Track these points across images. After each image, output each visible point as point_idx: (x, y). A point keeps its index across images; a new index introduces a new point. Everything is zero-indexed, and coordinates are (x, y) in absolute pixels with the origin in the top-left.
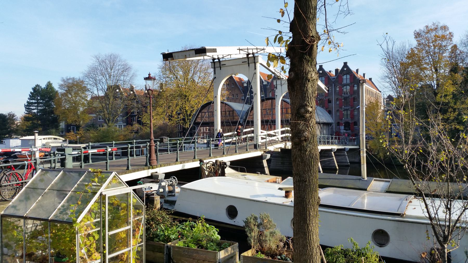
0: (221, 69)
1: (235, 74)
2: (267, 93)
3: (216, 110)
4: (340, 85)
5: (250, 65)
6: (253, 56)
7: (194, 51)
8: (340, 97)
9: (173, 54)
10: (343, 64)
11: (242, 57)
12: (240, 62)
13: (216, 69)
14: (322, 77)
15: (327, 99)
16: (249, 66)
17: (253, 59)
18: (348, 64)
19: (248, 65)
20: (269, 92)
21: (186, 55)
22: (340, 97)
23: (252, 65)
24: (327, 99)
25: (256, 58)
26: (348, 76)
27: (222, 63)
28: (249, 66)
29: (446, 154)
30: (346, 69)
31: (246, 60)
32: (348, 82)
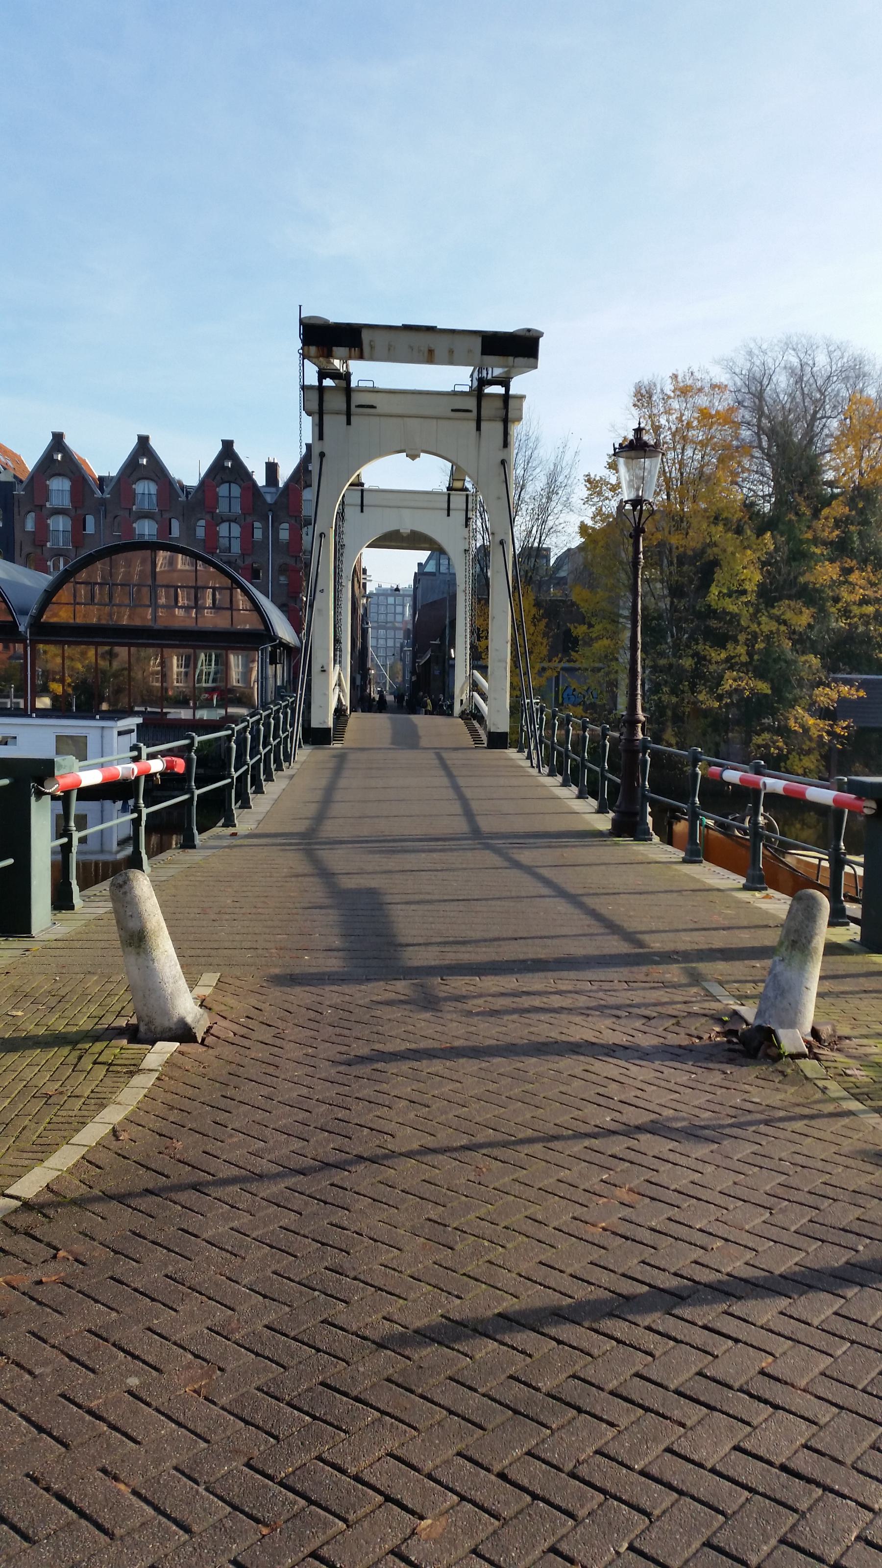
0: (349, 422)
1: (413, 452)
2: (16, 517)
3: (322, 591)
4: (293, 522)
5: (484, 425)
6: (503, 392)
7: (478, 343)
8: (291, 562)
9: (366, 336)
10: (220, 447)
11: (449, 389)
12: (448, 403)
13: (326, 418)
14: (230, 482)
15: (246, 563)
16: (478, 428)
17: (500, 404)
18: (237, 448)
19: (473, 425)
20: (22, 513)
21: (433, 347)
22: (291, 562)
23: (492, 429)
24: (246, 563)
25: (512, 403)
26: (236, 490)
27: (356, 399)
28: (478, 428)
29: (783, 769)
30: (145, 463)
31: (471, 403)
32: (237, 509)
